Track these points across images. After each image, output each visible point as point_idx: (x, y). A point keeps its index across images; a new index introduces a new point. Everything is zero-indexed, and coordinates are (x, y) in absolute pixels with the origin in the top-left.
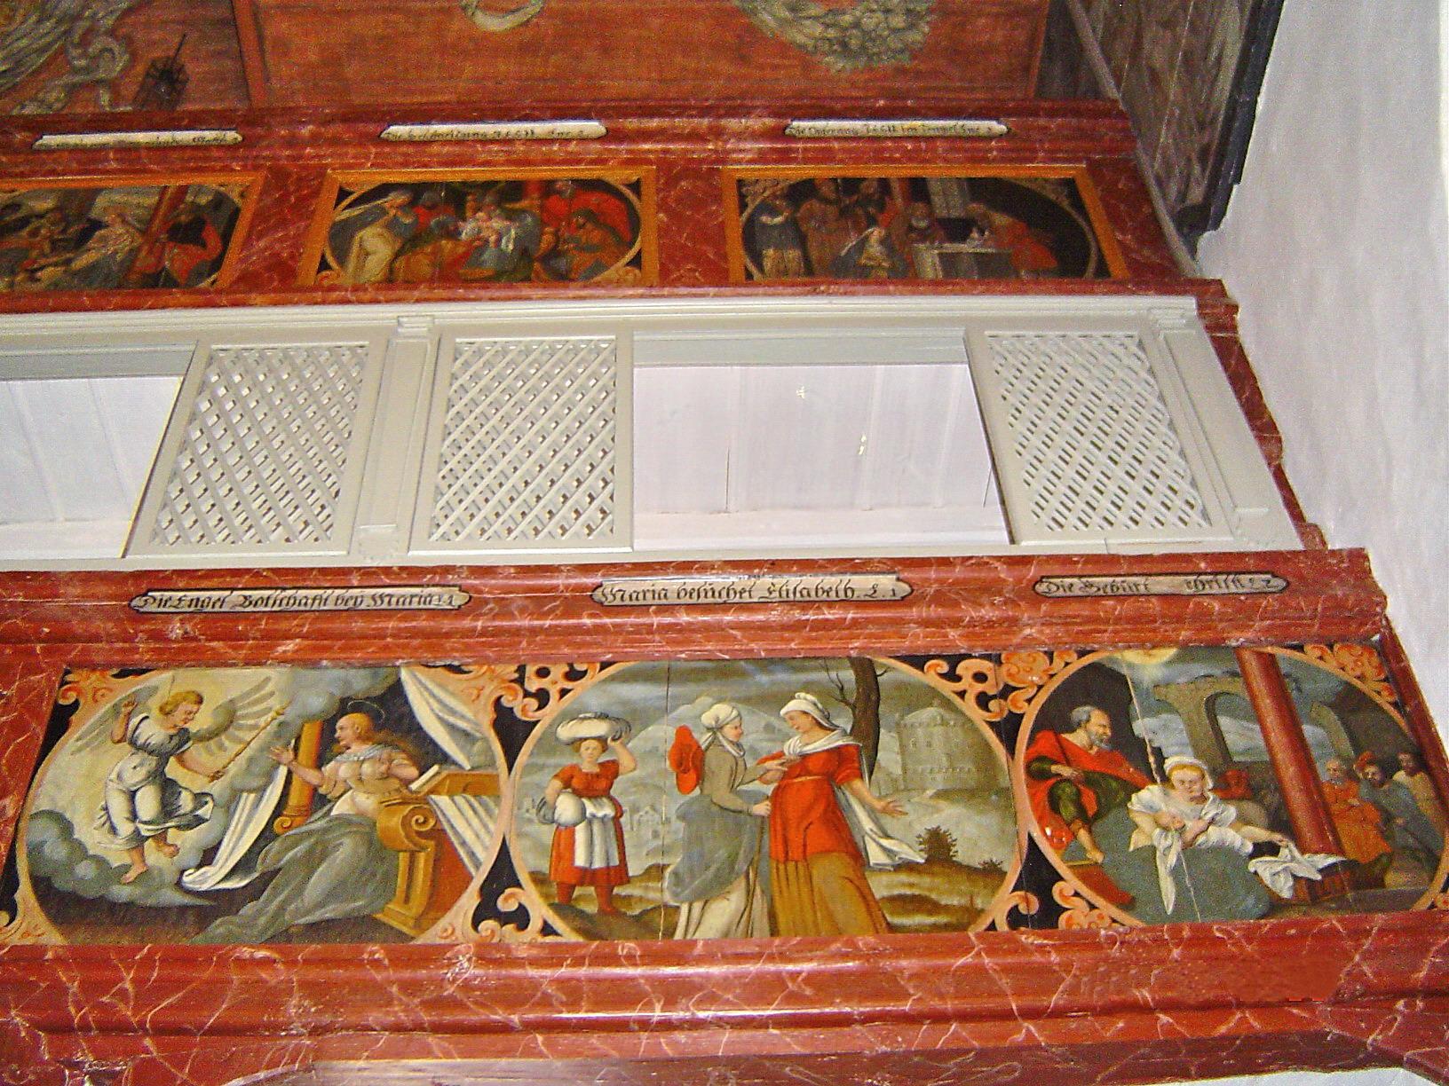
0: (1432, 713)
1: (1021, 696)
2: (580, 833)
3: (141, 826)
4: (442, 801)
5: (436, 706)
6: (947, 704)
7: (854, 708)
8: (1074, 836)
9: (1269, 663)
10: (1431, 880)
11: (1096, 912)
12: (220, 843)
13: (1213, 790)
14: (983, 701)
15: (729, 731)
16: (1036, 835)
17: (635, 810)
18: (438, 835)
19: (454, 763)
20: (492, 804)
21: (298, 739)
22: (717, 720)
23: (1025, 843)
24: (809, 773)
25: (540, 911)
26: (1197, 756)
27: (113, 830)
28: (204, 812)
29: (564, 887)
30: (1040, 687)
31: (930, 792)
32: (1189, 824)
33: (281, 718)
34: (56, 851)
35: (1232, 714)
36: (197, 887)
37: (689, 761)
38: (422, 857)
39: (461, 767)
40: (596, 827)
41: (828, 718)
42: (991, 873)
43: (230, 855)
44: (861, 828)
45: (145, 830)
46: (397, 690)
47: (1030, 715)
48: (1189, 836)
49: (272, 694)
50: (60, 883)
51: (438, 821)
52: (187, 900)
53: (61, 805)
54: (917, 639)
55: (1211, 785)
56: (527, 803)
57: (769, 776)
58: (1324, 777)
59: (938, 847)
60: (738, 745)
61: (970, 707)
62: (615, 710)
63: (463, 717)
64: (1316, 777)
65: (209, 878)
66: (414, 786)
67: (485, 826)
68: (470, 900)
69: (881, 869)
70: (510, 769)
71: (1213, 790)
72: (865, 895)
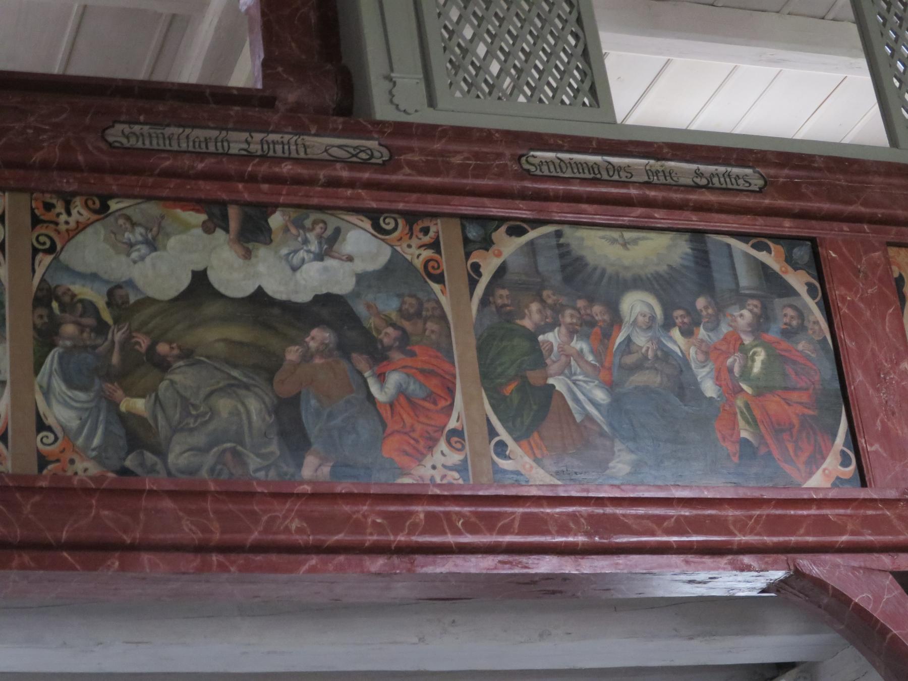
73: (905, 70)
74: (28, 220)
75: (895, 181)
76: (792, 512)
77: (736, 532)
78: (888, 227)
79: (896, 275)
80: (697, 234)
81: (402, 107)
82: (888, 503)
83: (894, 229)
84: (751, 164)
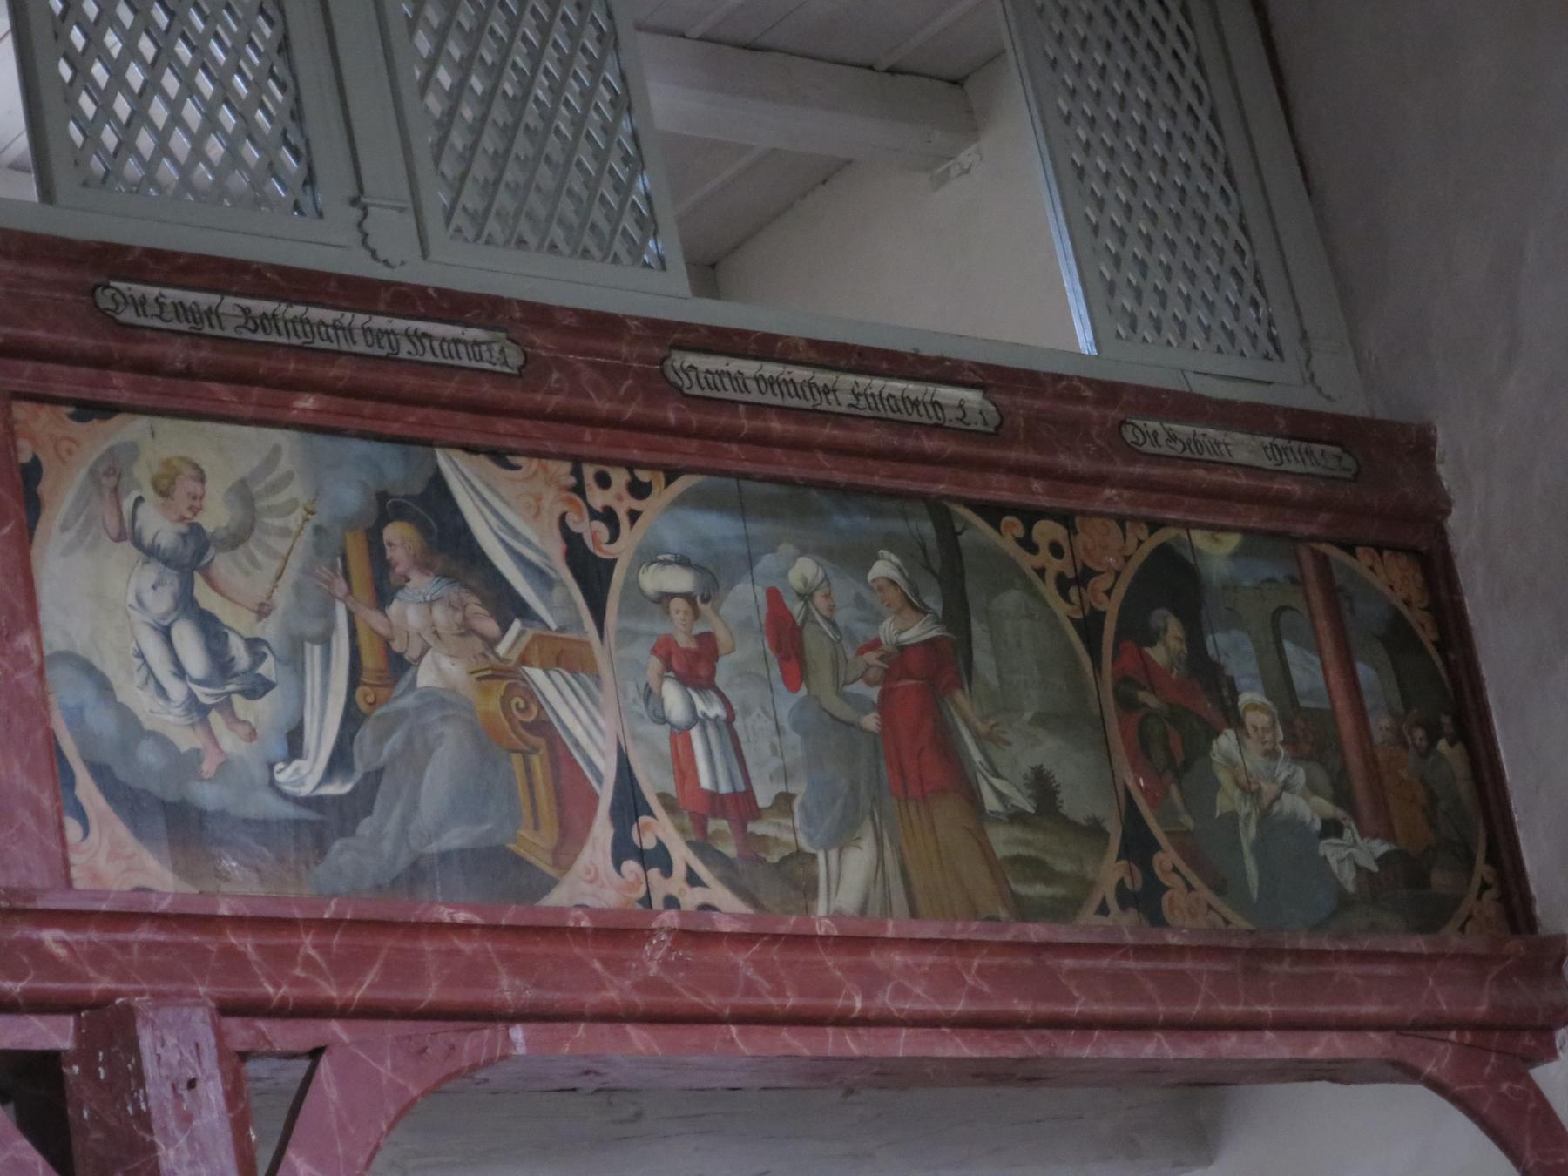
0: (1484, 673)
1: (1101, 583)
2: (695, 733)
3: (197, 689)
4: (536, 674)
5: (493, 520)
6: (1029, 586)
7: (940, 581)
8: (1167, 792)
9: (1323, 562)
10: (1469, 884)
11: (1193, 894)
12: (302, 721)
13: (1284, 743)
14: (1063, 584)
15: (819, 599)
16: (1130, 784)
17: (747, 711)
18: (543, 727)
19: (542, 622)
20: (592, 686)
21: (344, 558)
22: (805, 583)
23: (1122, 794)
24: (910, 676)
25: (681, 854)
26: (1268, 696)
27: (162, 691)
28: (267, 668)
29: (699, 811)
30: (1118, 574)
31: (1028, 716)
32: (1265, 786)
33: (314, 520)
34: (102, 722)
35: (1296, 642)
36: (287, 788)
37: (787, 639)
38: (536, 761)
39: (548, 628)
40: (711, 731)
41: (917, 594)
42: (1095, 831)
43: (322, 736)
44: (971, 761)
45: (204, 695)
46: (438, 481)
47: (1111, 608)
48: (1265, 802)
49: (289, 477)
50: (121, 773)
51: (541, 708)
52: (289, 811)
53: (81, 646)
54: (1001, 490)
55: (1281, 737)
56: (632, 692)
57: (871, 674)
58: (1378, 738)
59: (1042, 785)
60: (833, 624)
61: (1049, 590)
62: (695, 554)
63: (528, 543)
64: (1370, 738)
65: (305, 776)
66: (502, 649)
67: (594, 721)
68: (602, 831)
69: (996, 819)
70: (601, 636)
71: (1284, 743)
72: (986, 851)
73: (86, 48)
74: (640, 522)
75: (41, 272)
76: (196, 938)
77: (92, 973)
78: (21, 363)
79: (25, 458)
80: (939, 511)
81: (381, 255)
82: (1181, 951)
83: (29, 367)
84: (382, 308)
